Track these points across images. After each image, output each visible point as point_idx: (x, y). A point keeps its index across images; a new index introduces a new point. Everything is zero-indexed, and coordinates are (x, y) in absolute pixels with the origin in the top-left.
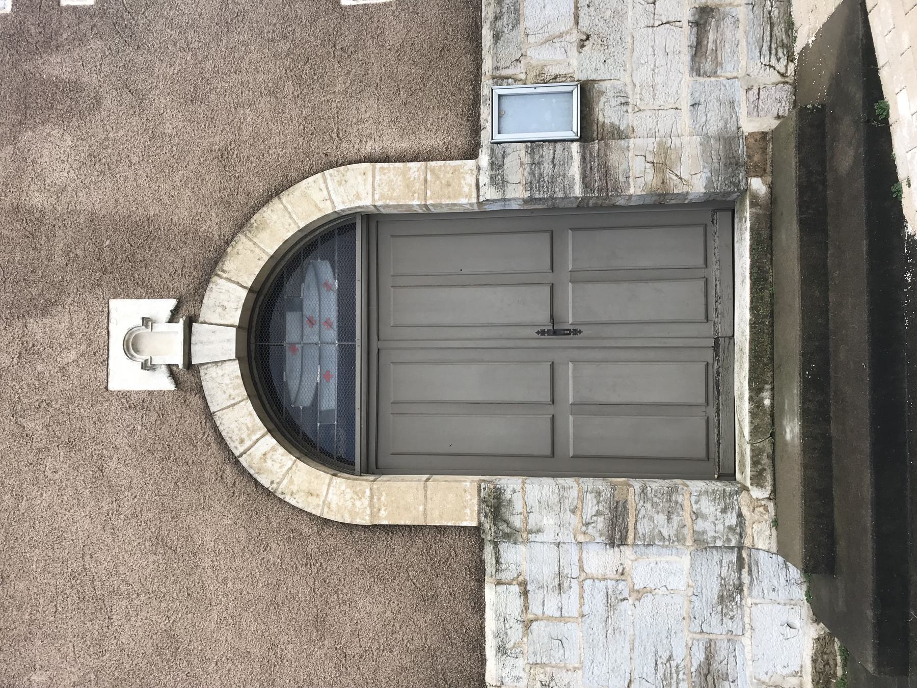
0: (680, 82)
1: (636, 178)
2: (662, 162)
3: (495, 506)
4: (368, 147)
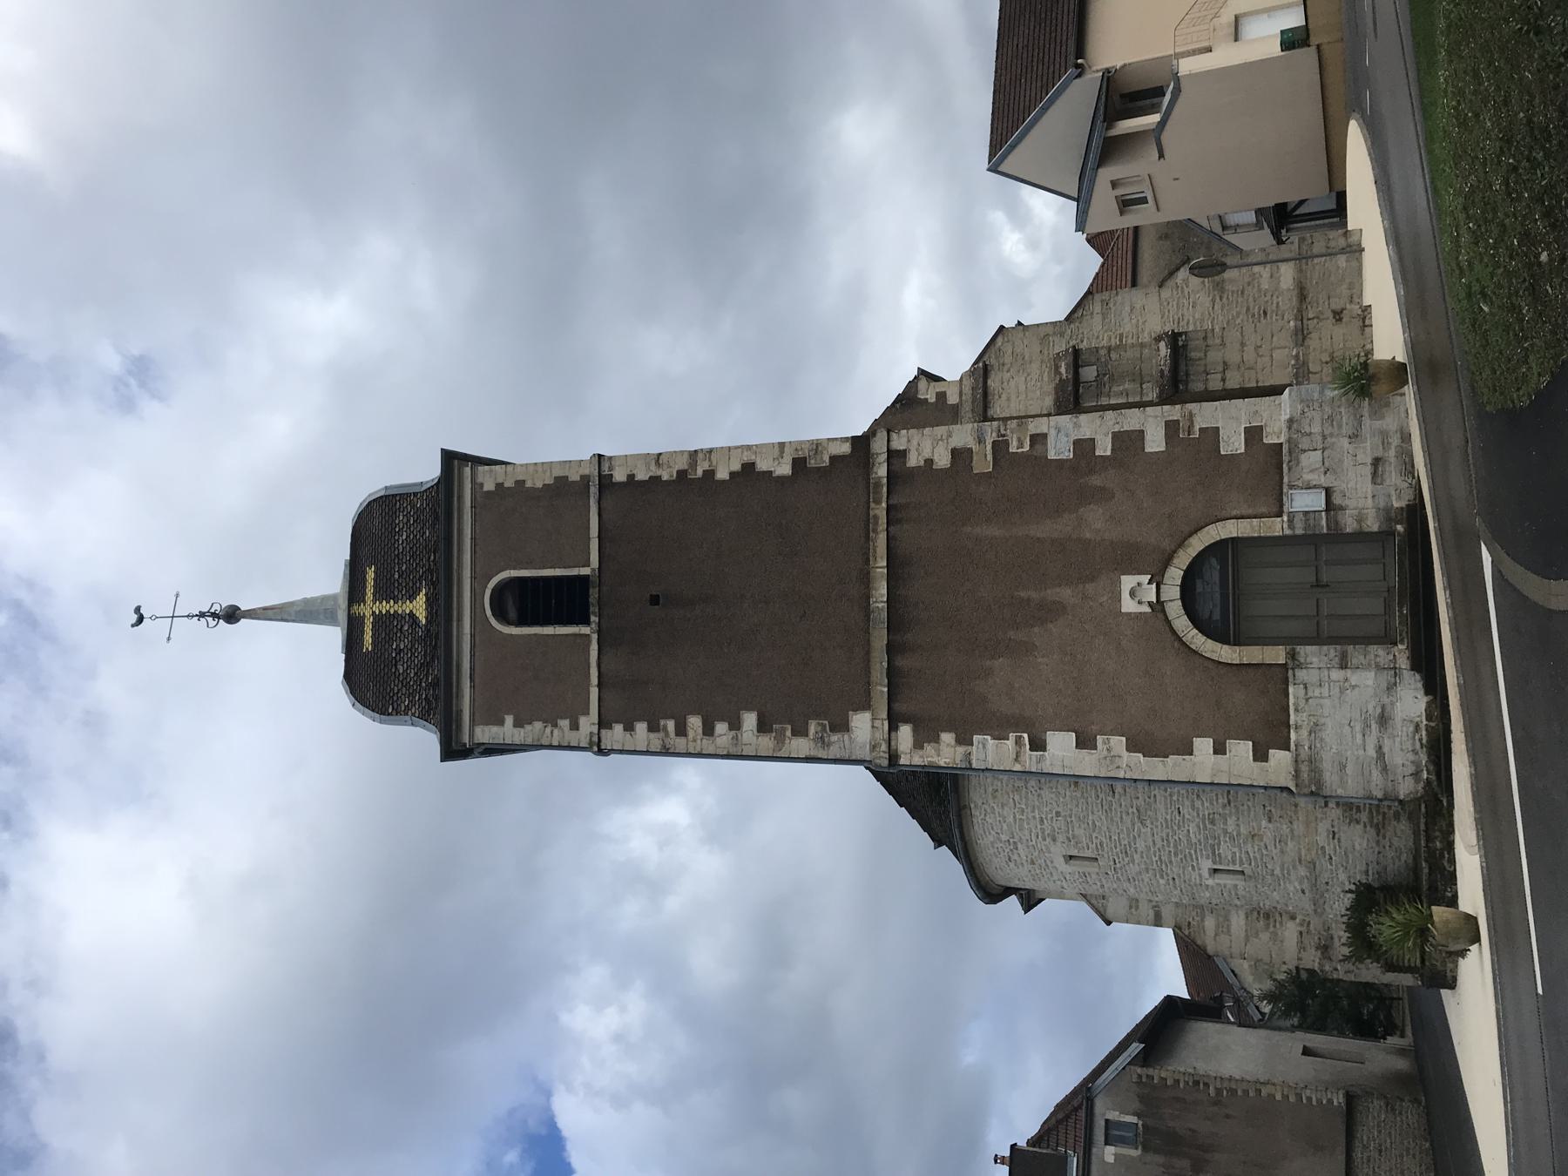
0: (1368, 487)
1: (1349, 524)
2: (1360, 519)
3: (1293, 655)
4: (1234, 513)
